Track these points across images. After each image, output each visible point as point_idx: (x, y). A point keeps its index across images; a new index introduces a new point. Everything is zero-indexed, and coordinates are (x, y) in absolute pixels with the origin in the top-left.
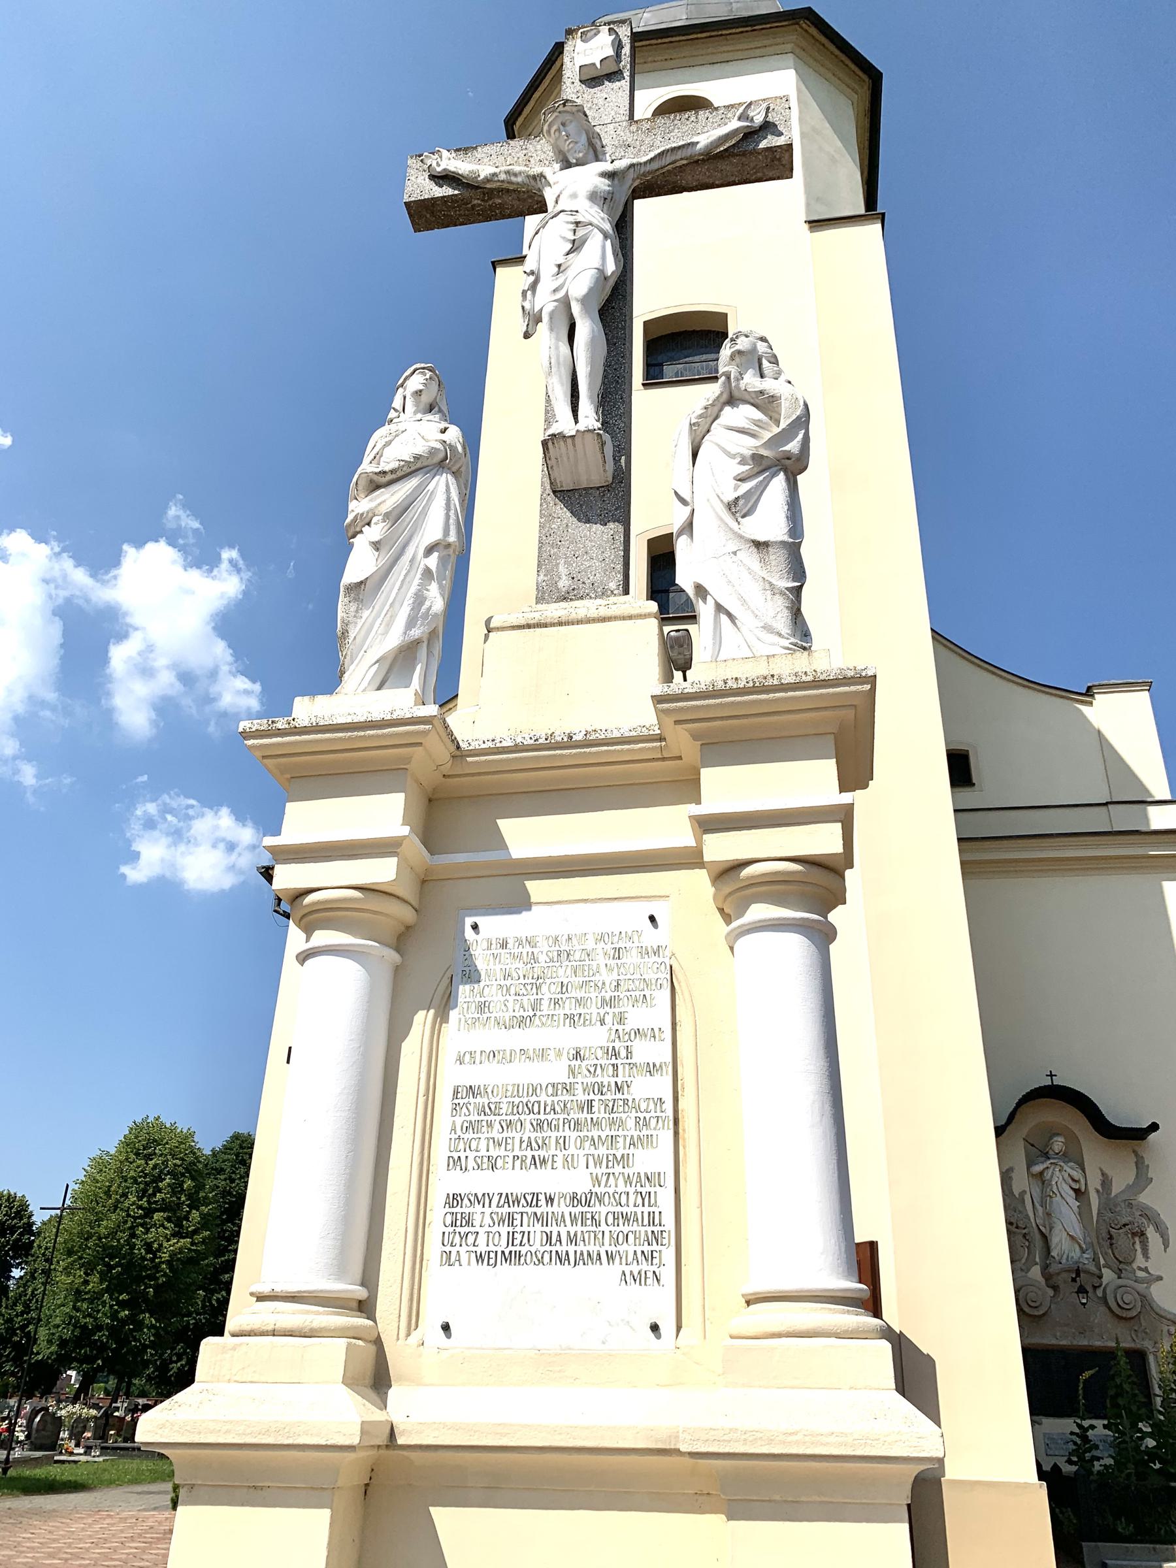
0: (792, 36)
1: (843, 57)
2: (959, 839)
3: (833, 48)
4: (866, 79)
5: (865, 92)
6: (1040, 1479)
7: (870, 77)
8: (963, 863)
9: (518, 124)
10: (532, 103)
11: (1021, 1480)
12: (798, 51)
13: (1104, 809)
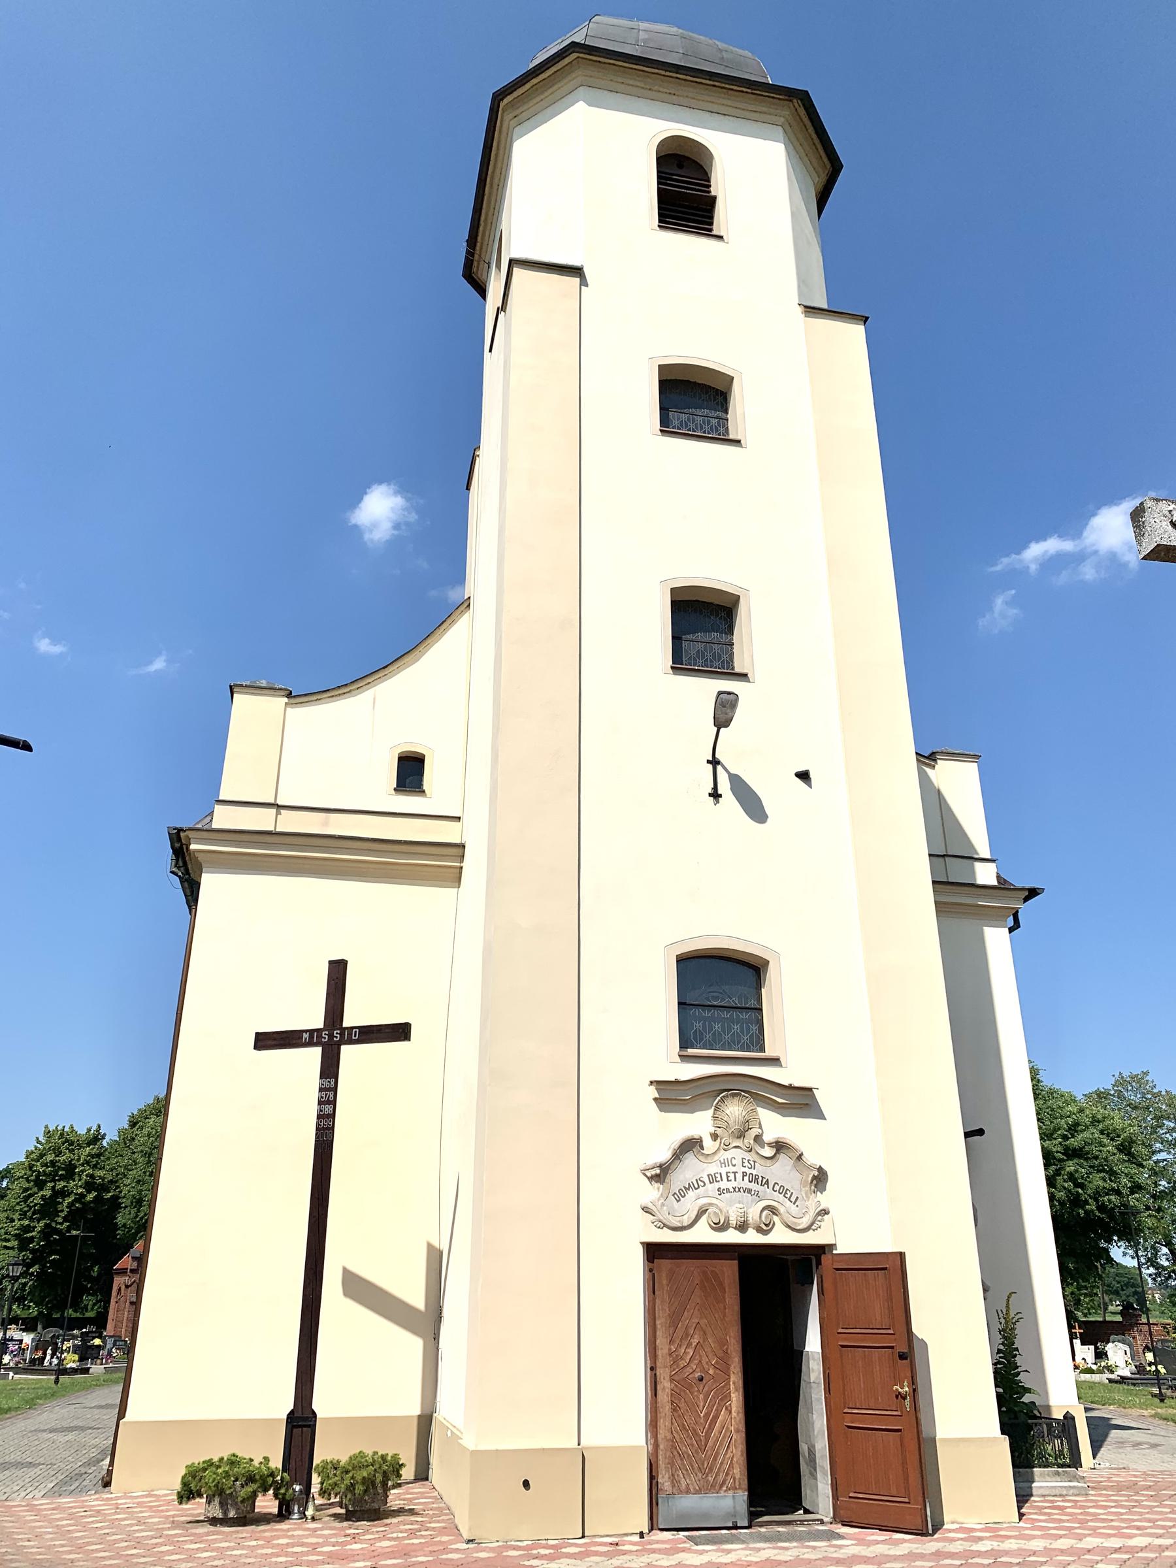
0: (785, 112)
1: (817, 141)
2: (934, 882)
3: (811, 130)
4: (828, 166)
5: (824, 178)
6: (1003, 1433)
7: (833, 165)
8: (936, 902)
9: (506, 101)
10: (528, 86)
11: (992, 1436)
12: (787, 127)
13: (941, 860)
